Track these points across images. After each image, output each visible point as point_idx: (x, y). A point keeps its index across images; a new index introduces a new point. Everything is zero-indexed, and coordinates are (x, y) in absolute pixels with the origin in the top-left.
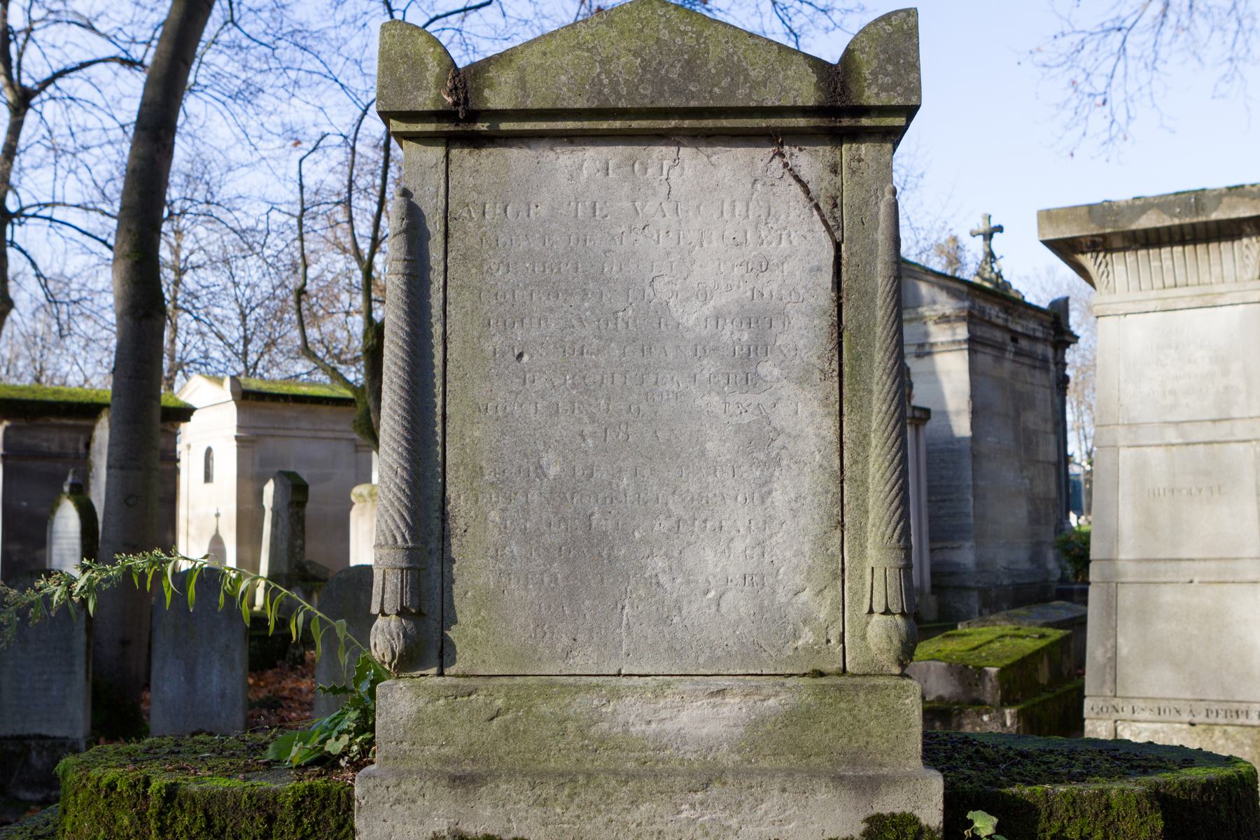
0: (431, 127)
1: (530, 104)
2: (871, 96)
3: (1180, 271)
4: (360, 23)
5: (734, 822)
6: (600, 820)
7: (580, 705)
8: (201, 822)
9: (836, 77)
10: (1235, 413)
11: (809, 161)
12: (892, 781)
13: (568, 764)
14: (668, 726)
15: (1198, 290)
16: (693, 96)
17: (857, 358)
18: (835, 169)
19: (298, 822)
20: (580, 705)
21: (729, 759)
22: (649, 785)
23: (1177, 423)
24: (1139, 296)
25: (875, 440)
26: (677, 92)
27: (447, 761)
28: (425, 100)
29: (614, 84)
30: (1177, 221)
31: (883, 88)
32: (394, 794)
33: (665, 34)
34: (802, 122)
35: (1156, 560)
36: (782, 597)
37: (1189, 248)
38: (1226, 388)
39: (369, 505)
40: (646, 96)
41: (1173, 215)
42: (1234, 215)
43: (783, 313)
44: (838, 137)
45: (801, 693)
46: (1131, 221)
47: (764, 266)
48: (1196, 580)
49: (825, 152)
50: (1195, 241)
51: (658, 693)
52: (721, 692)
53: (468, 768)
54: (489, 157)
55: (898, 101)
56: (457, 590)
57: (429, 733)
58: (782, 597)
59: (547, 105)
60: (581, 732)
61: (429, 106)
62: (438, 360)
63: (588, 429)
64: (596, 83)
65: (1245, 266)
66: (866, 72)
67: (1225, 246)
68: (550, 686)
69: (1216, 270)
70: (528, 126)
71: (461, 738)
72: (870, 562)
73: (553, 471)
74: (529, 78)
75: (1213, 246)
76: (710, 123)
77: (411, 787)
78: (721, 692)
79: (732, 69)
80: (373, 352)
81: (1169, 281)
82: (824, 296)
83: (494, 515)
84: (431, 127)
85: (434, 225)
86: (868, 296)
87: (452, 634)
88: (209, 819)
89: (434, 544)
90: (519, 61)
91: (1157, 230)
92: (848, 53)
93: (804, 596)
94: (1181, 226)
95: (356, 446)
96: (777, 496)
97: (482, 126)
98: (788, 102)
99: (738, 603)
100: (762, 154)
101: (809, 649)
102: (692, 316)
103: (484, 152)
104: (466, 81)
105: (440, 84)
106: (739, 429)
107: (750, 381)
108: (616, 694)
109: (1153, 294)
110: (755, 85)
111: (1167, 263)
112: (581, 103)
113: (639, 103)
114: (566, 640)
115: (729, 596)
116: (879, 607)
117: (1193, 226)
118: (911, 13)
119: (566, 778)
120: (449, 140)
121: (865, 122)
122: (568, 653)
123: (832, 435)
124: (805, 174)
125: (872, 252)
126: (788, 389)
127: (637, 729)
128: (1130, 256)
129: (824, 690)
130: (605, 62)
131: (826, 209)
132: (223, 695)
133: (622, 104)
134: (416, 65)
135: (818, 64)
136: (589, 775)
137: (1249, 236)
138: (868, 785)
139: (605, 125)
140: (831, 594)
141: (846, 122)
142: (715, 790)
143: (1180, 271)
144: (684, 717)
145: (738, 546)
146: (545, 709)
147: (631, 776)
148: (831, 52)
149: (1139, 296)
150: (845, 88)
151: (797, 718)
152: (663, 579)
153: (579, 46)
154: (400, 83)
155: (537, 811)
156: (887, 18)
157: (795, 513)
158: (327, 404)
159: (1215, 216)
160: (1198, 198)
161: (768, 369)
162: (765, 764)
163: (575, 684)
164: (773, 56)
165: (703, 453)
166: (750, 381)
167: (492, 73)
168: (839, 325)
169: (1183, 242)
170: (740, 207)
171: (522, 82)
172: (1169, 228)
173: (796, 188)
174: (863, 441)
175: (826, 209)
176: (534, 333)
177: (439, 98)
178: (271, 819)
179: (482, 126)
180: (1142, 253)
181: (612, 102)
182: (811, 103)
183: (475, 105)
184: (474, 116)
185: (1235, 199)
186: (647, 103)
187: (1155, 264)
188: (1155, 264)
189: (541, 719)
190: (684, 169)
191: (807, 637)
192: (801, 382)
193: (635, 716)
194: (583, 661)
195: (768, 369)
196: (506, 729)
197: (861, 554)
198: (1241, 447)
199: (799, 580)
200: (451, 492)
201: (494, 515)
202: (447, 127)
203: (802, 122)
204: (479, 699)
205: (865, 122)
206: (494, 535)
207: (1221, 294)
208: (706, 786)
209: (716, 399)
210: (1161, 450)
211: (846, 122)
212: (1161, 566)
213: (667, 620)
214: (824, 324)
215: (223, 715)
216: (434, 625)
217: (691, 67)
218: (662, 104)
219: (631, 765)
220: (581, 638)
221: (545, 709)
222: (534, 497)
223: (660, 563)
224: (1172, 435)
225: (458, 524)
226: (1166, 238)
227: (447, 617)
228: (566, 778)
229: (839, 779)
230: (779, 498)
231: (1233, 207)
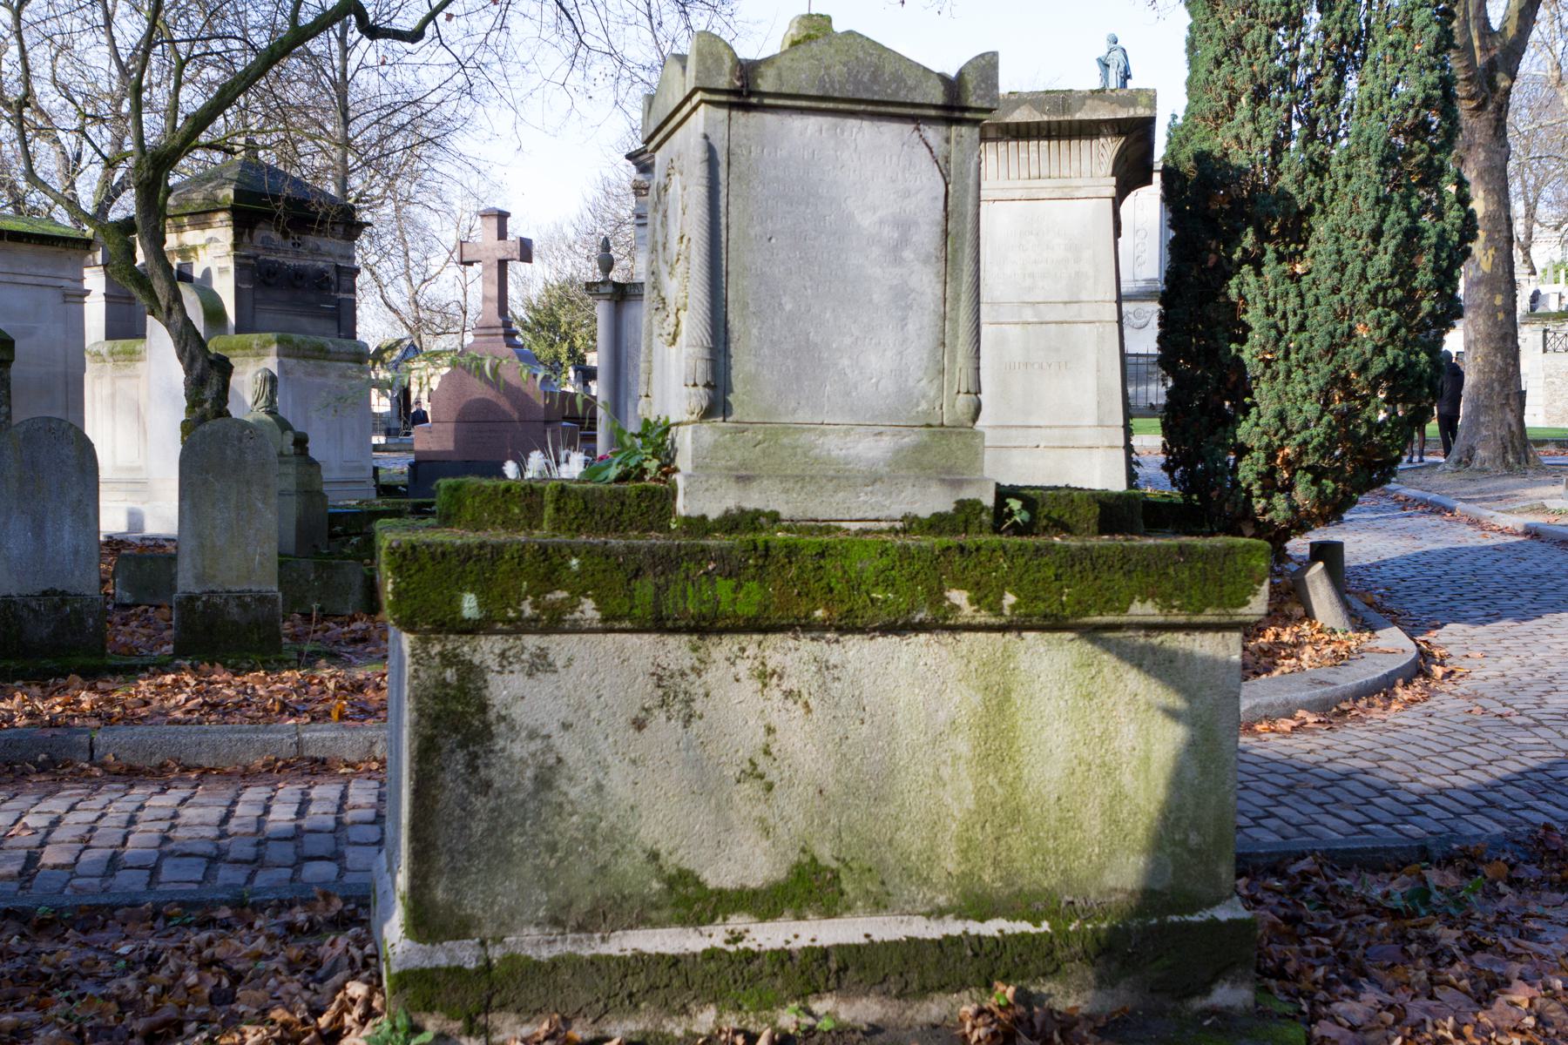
0: (723, 98)
1: (785, 90)
2: (973, 101)
3: (1044, 164)
4: (1142, 233)
5: (887, 503)
6: (817, 501)
7: (804, 439)
8: (581, 505)
9: (955, 86)
10: (1084, 296)
11: (933, 134)
12: (969, 482)
13: (797, 472)
14: (852, 452)
15: (1061, 182)
16: (875, 93)
17: (955, 251)
18: (948, 140)
19: (639, 506)
20: (804, 439)
21: (884, 470)
22: (844, 482)
23: (1033, 304)
24: (1008, 184)
25: (964, 297)
26: (867, 90)
27: (730, 469)
28: (723, 82)
29: (832, 83)
30: (1045, 118)
31: (979, 97)
32: (705, 485)
33: (861, 54)
34: (933, 113)
35: (1008, 427)
36: (911, 383)
37: (1054, 143)
38: (1077, 273)
39: (109, 365)
40: (849, 91)
41: (1043, 112)
42: (1094, 117)
43: (916, 223)
44: (950, 122)
45: (923, 435)
46: (1006, 115)
47: (907, 194)
48: (1042, 445)
49: (942, 129)
50: (1059, 137)
51: (847, 433)
52: (880, 434)
53: (743, 473)
54: (755, 118)
55: (986, 105)
56: (733, 373)
57: (721, 453)
58: (911, 383)
59: (794, 91)
60: (805, 455)
61: (726, 86)
62: (724, 239)
63: (808, 284)
64: (822, 80)
65: (1100, 163)
66: (970, 87)
67: (1085, 143)
68: (787, 429)
69: (1075, 164)
70: (780, 102)
71: (738, 455)
72: (959, 365)
73: (788, 307)
74: (784, 74)
75: (1075, 143)
76: (882, 109)
77: (714, 482)
78: (880, 434)
79: (898, 79)
80: (148, 186)
81: (1034, 172)
82: (938, 214)
83: (755, 331)
84: (723, 98)
85: (722, 157)
86: (963, 215)
87: (731, 398)
88: (586, 503)
89: (721, 347)
90: (778, 63)
91: (1028, 124)
92: (961, 74)
93: (923, 383)
94: (1049, 123)
95: (65, 295)
96: (910, 326)
97: (754, 100)
98: (927, 101)
99: (888, 386)
100: (908, 128)
101: (924, 412)
102: (866, 221)
103: (752, 114)
104: (748, 70)
105: (732, 72)
106: (891, 288)
107: (898, 261)
108: (824, 433)
109: (1020, 183)
110: (911, 89)
111: (1034, 156)
112: (813, 92)
113: (845, 95)
114: (793, 404)
115: (883, 382)
116: (963, 389)
117: (1059, 122)
118: (995, 54)
119: (799, 478)
120: (731, 106)
121: (967, 115)
122: (795, 410)
123: (940, 293)
124: (932, 142)
125: (966, 191)
126: (918, 266)
127: (835, 453)
128: (1002, 146)
129: (934, 434)
130: (827, 68)
131: (941, 163)
132: (76, 552)
133: (836, 94)
134: (718, 60)
135: (943, 78)
136: (812, 477)
137: (1105, 136)
138: (957, 484)
139: (823, 105)
140: (936, 382)
141: (957, 114)
142: (878, 485)
143: (1044, 164)
144: (860, 447)
145: (889, 354)
146: (786, 441)
147: (832, 479)
148: (952, 73)
149: (1008, 184)
150: (959, 96)
151: (921, 448)
152: (848, 371)
153: (812, 57)
154: (708, 69)
155: (784, 496)
156: (982, 56)
157: (919, 336)
158: (29, 242)
159: (1078, 116)
160: (1063, 99)
161: (908, 254)
162: (902, 473)
163: (799, 428)
164: (920, 73)
165: (871, 301)
166: (898, 261)
167: (763, 69)
168: (946, 233)
169: (1049, 138)
170: (895, 159)
171: (779, 76)
172: (1038, 123)
173: (926, 150)
174: (957, 298)
175: (941, 163)
176: (779, 226)
177: (731, 82)
178: (623, 504)
179: (754, 100)
180: (1013, 144)
181: (831, 93)
182: (940, 102)
183: (752, 87)
184: (751, 94)
185: (1096, 102)
186: (850, 95)
187: (1023, 155)
188: (1023, 155)
189: (783, 447)
190: (862, 133)
191: (924, 406)
192: (926, 261)
193: (834, 446)
194: (803, 416)
195: (908, 254)
196: (764, 452)
197: (953, 360)
198: (1087, 327)
199: (920, 374)
200: (730, 316)
201: (755, 331)
202: (733, 99)
203: (933, 113)
204: (748, 434)
205: (967, 115)
206: (755, 343)
207: (1078, 188)
208: (873, 483)
209: (879, 270)
210: (1019, 327)
211: (957, 114)
212: (1014, 432)
213: (848, 394)
214: (938, 230)
215: (77, 573)
216: (721, 393)
217: (875, 77)
218: (858, 96)
219: (831, 473)
220: (803, 402)
221: (786, 441)
222: (778, 321)
223: (845, 362)
224: (1028, 314)
225: (734, 336)
226: (1034, 132)
227: (728, 389)
228: (799, 478)
229: (943, 481)
230: (911, 327)
231: (1094, 110)
